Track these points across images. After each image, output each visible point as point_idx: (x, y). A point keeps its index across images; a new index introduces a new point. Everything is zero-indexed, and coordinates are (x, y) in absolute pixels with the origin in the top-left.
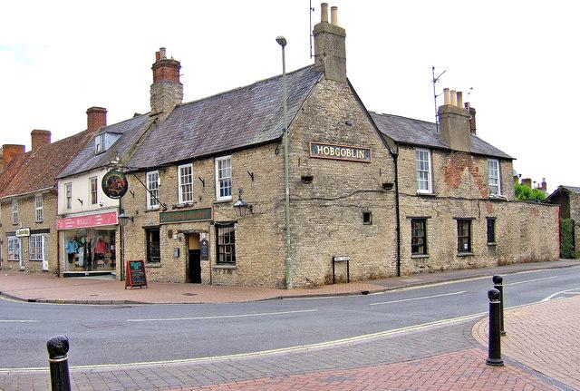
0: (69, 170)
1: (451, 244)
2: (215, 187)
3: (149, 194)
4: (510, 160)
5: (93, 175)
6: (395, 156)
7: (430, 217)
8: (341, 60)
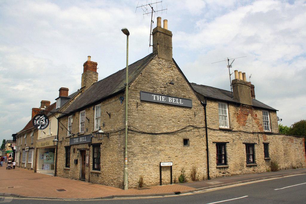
1: (242, 159)
4: (274, 111)
6: (204, 105)
7: (228, 142)
8: (168, 48)
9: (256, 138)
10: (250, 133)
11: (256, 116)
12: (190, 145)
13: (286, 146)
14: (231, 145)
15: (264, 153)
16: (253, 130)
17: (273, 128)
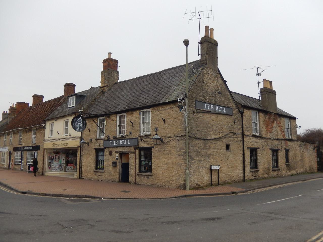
0: (47, 118)
1: (269, 163)
2: (140, 127)
3: (98, 130)
4: (294, 118)
5: (65, 119)
6: (242, 113)
7: (259, 148)
9: (280, 144)
10: (274, 139)
11: (280, 124)
12: (231, 151)
13: (302, 152)
14: (261, 150)
15: (285, 158)
16: (278, 137)
17: (293, 135)
